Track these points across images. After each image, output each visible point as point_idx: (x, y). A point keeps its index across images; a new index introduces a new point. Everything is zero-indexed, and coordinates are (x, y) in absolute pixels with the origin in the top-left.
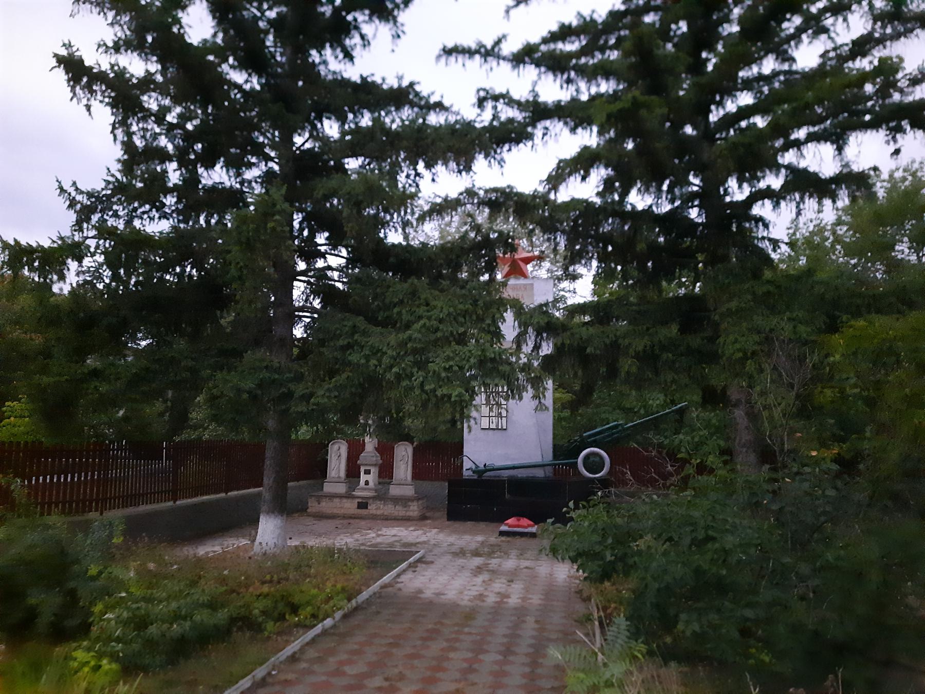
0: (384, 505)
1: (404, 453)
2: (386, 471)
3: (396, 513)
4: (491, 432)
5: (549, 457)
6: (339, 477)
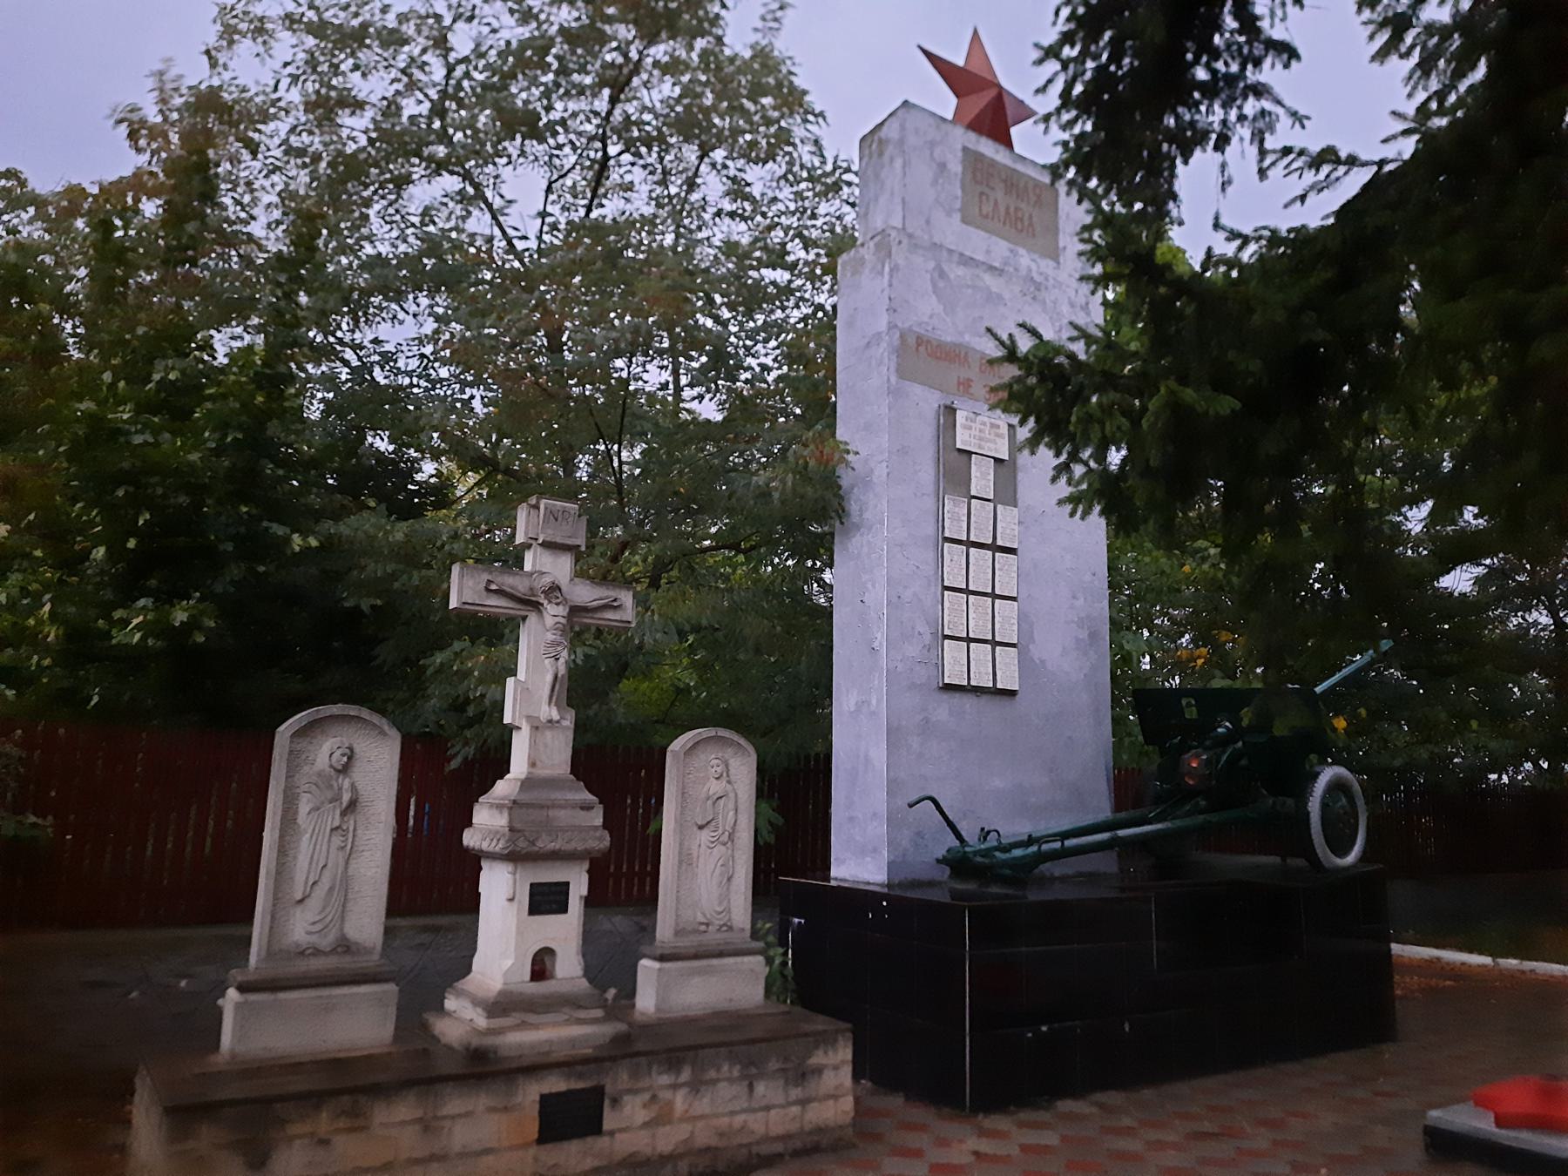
0: (696, 1086)
1: (715, 787)
2: (625, 878)
3: (757, 1124)
4: (968, 701)
5: (1101, 808)
6: (345, 946)
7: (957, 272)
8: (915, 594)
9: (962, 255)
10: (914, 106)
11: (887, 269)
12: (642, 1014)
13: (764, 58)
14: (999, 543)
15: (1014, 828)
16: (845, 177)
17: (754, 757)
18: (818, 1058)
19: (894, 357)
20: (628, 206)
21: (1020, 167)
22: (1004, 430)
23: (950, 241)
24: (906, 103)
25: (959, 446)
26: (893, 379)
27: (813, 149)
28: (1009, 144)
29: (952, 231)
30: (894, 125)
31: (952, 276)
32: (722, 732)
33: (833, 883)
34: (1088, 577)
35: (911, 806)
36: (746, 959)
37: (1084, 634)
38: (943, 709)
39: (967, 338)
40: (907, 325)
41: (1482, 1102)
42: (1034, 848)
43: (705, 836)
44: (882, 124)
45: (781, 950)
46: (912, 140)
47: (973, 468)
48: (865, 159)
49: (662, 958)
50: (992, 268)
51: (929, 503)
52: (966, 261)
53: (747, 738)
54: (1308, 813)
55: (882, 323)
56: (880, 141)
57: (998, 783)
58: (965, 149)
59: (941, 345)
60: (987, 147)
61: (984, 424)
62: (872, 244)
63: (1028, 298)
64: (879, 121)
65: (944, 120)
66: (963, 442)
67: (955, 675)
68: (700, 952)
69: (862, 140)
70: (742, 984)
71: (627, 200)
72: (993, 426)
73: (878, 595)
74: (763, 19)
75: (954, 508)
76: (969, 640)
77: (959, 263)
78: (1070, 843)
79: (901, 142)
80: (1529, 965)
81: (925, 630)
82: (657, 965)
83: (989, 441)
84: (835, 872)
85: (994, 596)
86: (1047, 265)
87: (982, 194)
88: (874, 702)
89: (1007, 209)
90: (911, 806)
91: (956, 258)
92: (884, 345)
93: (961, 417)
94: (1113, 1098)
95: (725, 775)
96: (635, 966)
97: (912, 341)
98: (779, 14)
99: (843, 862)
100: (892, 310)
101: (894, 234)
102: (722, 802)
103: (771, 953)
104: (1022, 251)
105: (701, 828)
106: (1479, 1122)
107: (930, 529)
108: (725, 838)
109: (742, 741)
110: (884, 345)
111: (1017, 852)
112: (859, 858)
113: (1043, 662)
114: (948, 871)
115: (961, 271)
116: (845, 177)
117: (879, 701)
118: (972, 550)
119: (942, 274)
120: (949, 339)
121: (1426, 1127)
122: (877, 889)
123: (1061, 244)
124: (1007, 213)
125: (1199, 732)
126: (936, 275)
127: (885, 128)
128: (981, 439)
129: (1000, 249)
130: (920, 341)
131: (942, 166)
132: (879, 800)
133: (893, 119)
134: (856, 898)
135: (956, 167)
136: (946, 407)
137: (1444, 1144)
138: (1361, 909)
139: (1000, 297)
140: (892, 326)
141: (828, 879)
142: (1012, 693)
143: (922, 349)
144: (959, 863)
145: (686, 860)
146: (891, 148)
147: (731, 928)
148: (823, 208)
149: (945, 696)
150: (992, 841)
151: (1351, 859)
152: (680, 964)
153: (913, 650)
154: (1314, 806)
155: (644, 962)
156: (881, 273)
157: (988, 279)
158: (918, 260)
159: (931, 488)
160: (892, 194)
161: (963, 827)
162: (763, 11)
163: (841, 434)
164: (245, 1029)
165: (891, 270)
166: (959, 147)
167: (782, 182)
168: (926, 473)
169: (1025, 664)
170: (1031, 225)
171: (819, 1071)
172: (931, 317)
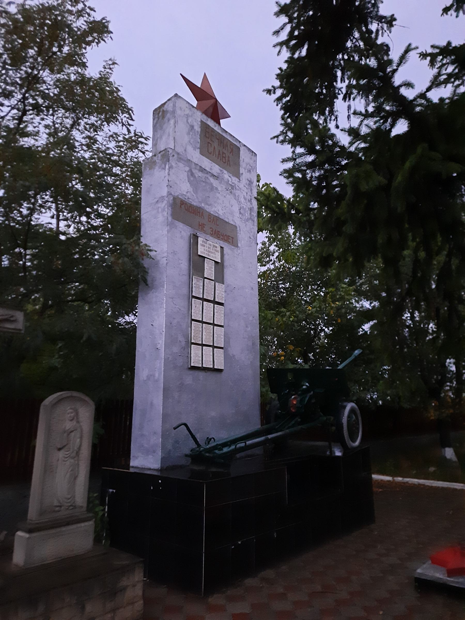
1: (69, 425)
4: (201, 375)
7: (198, 174)
8: (178, 322)
9: (201, 167)
10: (180, 97)
11: (167, 167)
12: (16, 566)
13: (104, 79)
14: (217, 300)
15: (222, 436)
16: (140, 139)
17: (94, 407)
18: (125, 582)
19: (170, 208)
20: (37, 143)
21: (224, 135)
22: (219, 249)
23: (195, 160)
24: (176, 95)
25: (199, 254)
26: (170, 219)
27: (127, 116)
28: (219, 124)
29: (195, 156)
30: (170, 104)
31: (197, 176)
32: (75, 394)
33: (132, 470)
34: (251, 318)
35: (175, 428)
36: (83, 525)
37: (250, 343)
38: (189, 378)
39: (203, 205)
40: (176, 195)
41: (436, 561)
42: (233, 447)
43: (61, 454)
44: (165, 104)
45: (102, 508)
46: (179, 112)
47: (206, 264)
48: (156, 119)
49: (30, 531)
50: (213, 176)
51: (185, 278)
52: (202, 170)
53: (87, 395)
54: (343, 424)
55: (164, 192)
56: (163, 111)
57: (213, 414)
58: (202, 122)
59: (191, 206)
60: (211, 123)
61: (210, 245)
62: (160, 155)
63: (228, 192)
64: (163, 103)
65: (193, 107)
66: (201, 252)
67: (195, 362)
68: (55, 522)
69: (154, 111)
70: (79, 540)
71: (36, 140)
72: (214, 246)
73: (161, 321)
74: (105, 68)
75: (197, 282)
76: (203, 345)
77: (200, 171)
78: (249, 443)
79: (174, 112)
80: (422, 481)
81: (181, 338)
82: (27, 535)
83: (212, 253)
84: (133, 463)
85: (214, 325)
86: (235, 180)
87: (209, 143)
88: (157, 375)
89: (219, 152)
90: (175, 428)
91: (198, 168)
92: (165, 202)
93: (200, 240)
94: (269, 573)
95: (76, 418)
96: (14, 535)
97: (178, 202)
98: (111, 66)
99: (136, 458)
100: (169, 186)
101: (171, 151)
102: (73, 434)
103: (97, 509)
104: (225, 172)
105: (60, 449)
106: (438, 574)
107: (185, 291)
108: (74, 454)
109: (87, 398)
110: (165, 202)
111: (225, 450)
112: (145, 457)
113: (234, 356)
114: (190, 460)
115: (200, 174)
116: (140, 139)
117: (160, 374)
118: (205, 303)
119: (192, 174)
120: (195, 204)
121: (416, 578)
122: (155, 473)
123: (241, 172)
124: (219, 154)
125: (295, 387)
126: (190, 174)
127: (166, 106)
128: (209, 252)
129: (216, 169)
130: (183, 203)
131: (192, 127)
132: (157, 425)
133: (170, 101)
134: (142, 478)
135: (197, 128)
136: (194, 235)
137: (425, 586)
138: (360, 462)
139: (217, 189)
140: (169, 194)
141: (128, 467)
142: (220, 371)
143: (183, 206)
144: (197, 457)
145: (48, 469)
146: (168, 115)
147: (75, 507)
148: (130, 154)
149: (191, 372)
150: (212, 444)
151: (357, 443)
152: (42, 533)
153: (176, 349)
154: (345, 420)
155: (19, 533)
156: (164, 169)
157: (212, 180)
158: (181, 165)
159: (186, 272)
160: (169, 135)
161: (198, 436)
162: (105, 64)
163: (144, 240)
164: (352, 80)
165: (169, 168)
166: (200, 120)
167: (111, 139)
168: (184, 265)
169: (227, 357)
170: (229, 161)
171: (124, 589)
172: (187, 193)
